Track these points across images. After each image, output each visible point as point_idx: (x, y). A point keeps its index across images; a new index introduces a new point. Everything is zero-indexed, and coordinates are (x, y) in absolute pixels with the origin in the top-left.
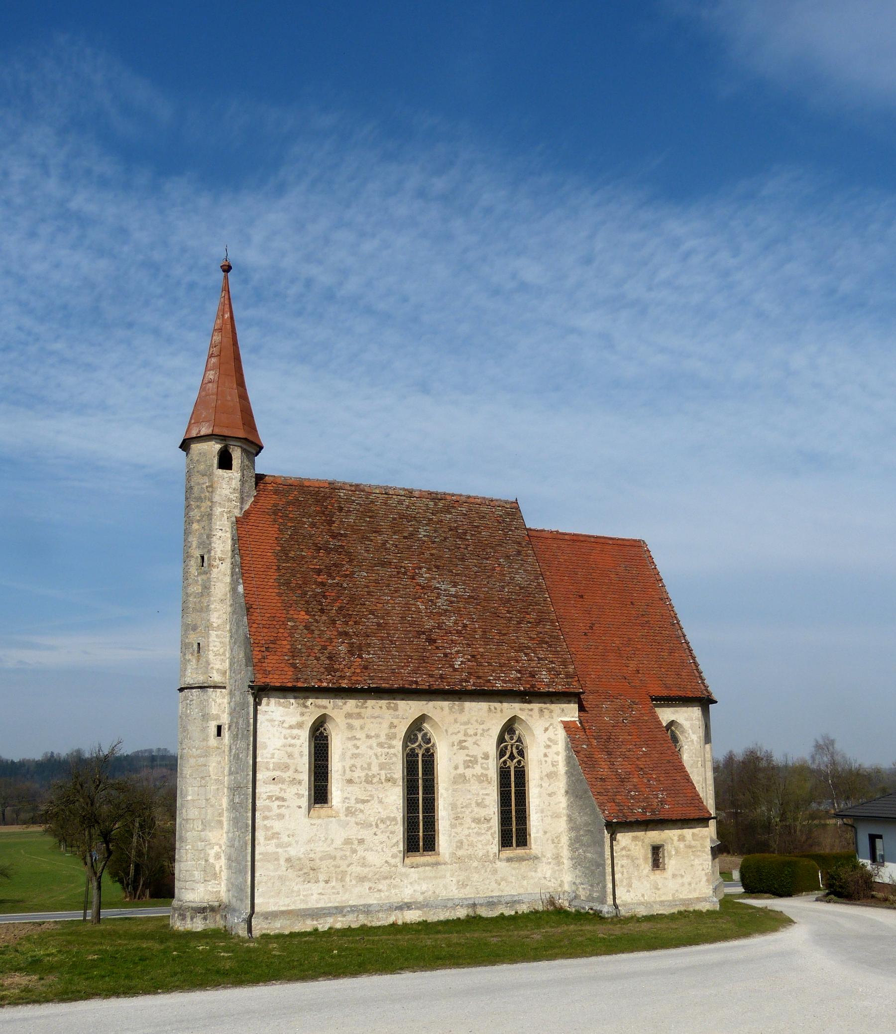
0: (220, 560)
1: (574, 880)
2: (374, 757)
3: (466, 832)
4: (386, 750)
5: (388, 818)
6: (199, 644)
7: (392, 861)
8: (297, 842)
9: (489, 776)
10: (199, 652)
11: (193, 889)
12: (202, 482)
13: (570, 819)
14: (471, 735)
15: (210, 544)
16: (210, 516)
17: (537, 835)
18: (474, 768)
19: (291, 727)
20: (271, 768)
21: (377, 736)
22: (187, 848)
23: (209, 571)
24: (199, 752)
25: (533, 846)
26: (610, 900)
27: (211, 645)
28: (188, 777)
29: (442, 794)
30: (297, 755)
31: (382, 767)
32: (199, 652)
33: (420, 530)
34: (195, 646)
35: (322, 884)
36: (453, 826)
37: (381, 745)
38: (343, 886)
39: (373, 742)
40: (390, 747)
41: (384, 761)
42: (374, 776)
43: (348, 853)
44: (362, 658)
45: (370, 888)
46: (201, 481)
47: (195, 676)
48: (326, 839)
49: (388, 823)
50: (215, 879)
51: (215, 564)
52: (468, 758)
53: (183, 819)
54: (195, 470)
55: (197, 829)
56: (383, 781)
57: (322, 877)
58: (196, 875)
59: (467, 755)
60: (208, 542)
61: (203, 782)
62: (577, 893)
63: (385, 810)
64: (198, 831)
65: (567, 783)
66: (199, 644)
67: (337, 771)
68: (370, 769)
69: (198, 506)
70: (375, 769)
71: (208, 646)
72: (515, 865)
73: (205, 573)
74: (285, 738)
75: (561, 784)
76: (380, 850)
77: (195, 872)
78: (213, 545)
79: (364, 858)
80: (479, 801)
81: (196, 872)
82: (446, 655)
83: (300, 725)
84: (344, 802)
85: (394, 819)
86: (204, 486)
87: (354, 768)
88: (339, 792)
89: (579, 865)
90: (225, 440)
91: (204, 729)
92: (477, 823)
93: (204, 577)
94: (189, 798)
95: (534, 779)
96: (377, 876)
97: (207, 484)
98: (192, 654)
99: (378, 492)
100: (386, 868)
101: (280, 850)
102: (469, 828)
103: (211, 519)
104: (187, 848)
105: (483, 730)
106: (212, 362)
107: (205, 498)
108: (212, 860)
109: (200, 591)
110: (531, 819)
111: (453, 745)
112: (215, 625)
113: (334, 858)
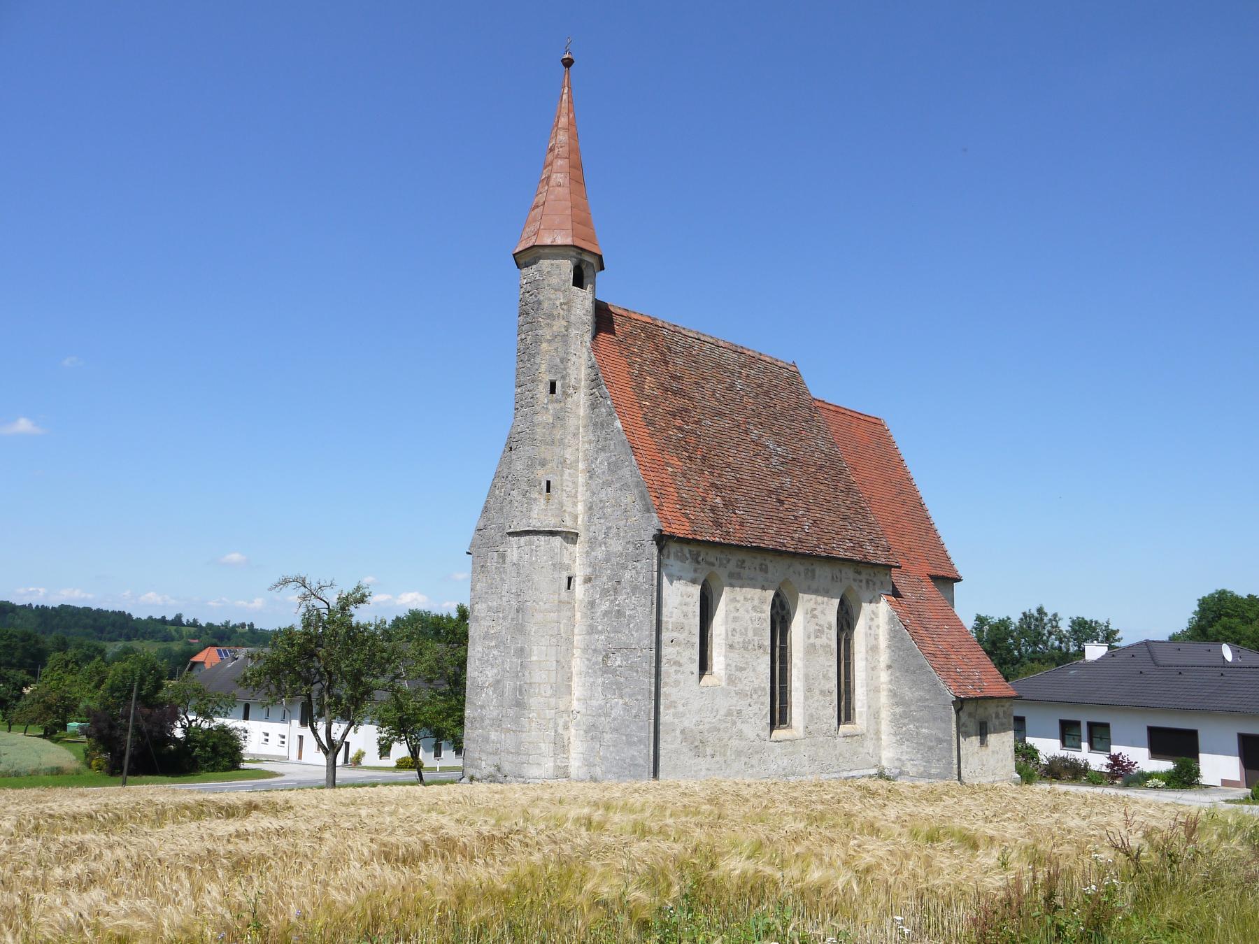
2: (749, 622)
3: (815, 705)
4: (760, 615)
5: (760, 687)
6: (548, 483)
8: (690, 711)
9: (832, 647)
10: (548, 490)
11: (538, 764)
13: (893, 694)
14: (819, 604)
15: (565, 369)
17: (862, 710)
18: (821, 638)
21: (752, 599)
22: (530, 716)
24: (547, 606)
28: (533, 634)
29: (795, 664)
30: (690, 615)
31: (756, 632)
32: (548, 490)
34: (544, 485)
35: (709, 758)
36: (806, 698)
37: (755, 609)
39: (749, 605)
41: (757, 626)
42: (749, 642)
43: (729, 725)
45: (745, 763)
46: (553, 297)
49: (760, 693)
52: (817, 627)
54: (546, 282)
55: (544, 694)
57: (709, 751)
58: (543, 748)
59: (817, 624)
60: (562, 367)
62: (903, 768)
63: (757, 678)
64: (546, 697)
65: (890, 657)
66: (548, 483)
67: (720, 635)
68: (746, 634)
69: (548, 324)
70: (750, 633)
73: (558, 401)
75: (884, 657)
81: (542, 745)
85: (764, 689)
86: (558, 303)
87: (734, 633)
88: (722, 659)
89: (908, 740)
90: (580, 254)
92: (824, 696)
93: (558, 406)
94: (534, 658)
95: (860, 652)
96: (751, 750)
97: (561, 301)
100: (757, 742)
101: (676, 721)
106: (559, 164)
107: (558, 317)
108: (560, 730)
109: (551, 421)
111: (807, 613)
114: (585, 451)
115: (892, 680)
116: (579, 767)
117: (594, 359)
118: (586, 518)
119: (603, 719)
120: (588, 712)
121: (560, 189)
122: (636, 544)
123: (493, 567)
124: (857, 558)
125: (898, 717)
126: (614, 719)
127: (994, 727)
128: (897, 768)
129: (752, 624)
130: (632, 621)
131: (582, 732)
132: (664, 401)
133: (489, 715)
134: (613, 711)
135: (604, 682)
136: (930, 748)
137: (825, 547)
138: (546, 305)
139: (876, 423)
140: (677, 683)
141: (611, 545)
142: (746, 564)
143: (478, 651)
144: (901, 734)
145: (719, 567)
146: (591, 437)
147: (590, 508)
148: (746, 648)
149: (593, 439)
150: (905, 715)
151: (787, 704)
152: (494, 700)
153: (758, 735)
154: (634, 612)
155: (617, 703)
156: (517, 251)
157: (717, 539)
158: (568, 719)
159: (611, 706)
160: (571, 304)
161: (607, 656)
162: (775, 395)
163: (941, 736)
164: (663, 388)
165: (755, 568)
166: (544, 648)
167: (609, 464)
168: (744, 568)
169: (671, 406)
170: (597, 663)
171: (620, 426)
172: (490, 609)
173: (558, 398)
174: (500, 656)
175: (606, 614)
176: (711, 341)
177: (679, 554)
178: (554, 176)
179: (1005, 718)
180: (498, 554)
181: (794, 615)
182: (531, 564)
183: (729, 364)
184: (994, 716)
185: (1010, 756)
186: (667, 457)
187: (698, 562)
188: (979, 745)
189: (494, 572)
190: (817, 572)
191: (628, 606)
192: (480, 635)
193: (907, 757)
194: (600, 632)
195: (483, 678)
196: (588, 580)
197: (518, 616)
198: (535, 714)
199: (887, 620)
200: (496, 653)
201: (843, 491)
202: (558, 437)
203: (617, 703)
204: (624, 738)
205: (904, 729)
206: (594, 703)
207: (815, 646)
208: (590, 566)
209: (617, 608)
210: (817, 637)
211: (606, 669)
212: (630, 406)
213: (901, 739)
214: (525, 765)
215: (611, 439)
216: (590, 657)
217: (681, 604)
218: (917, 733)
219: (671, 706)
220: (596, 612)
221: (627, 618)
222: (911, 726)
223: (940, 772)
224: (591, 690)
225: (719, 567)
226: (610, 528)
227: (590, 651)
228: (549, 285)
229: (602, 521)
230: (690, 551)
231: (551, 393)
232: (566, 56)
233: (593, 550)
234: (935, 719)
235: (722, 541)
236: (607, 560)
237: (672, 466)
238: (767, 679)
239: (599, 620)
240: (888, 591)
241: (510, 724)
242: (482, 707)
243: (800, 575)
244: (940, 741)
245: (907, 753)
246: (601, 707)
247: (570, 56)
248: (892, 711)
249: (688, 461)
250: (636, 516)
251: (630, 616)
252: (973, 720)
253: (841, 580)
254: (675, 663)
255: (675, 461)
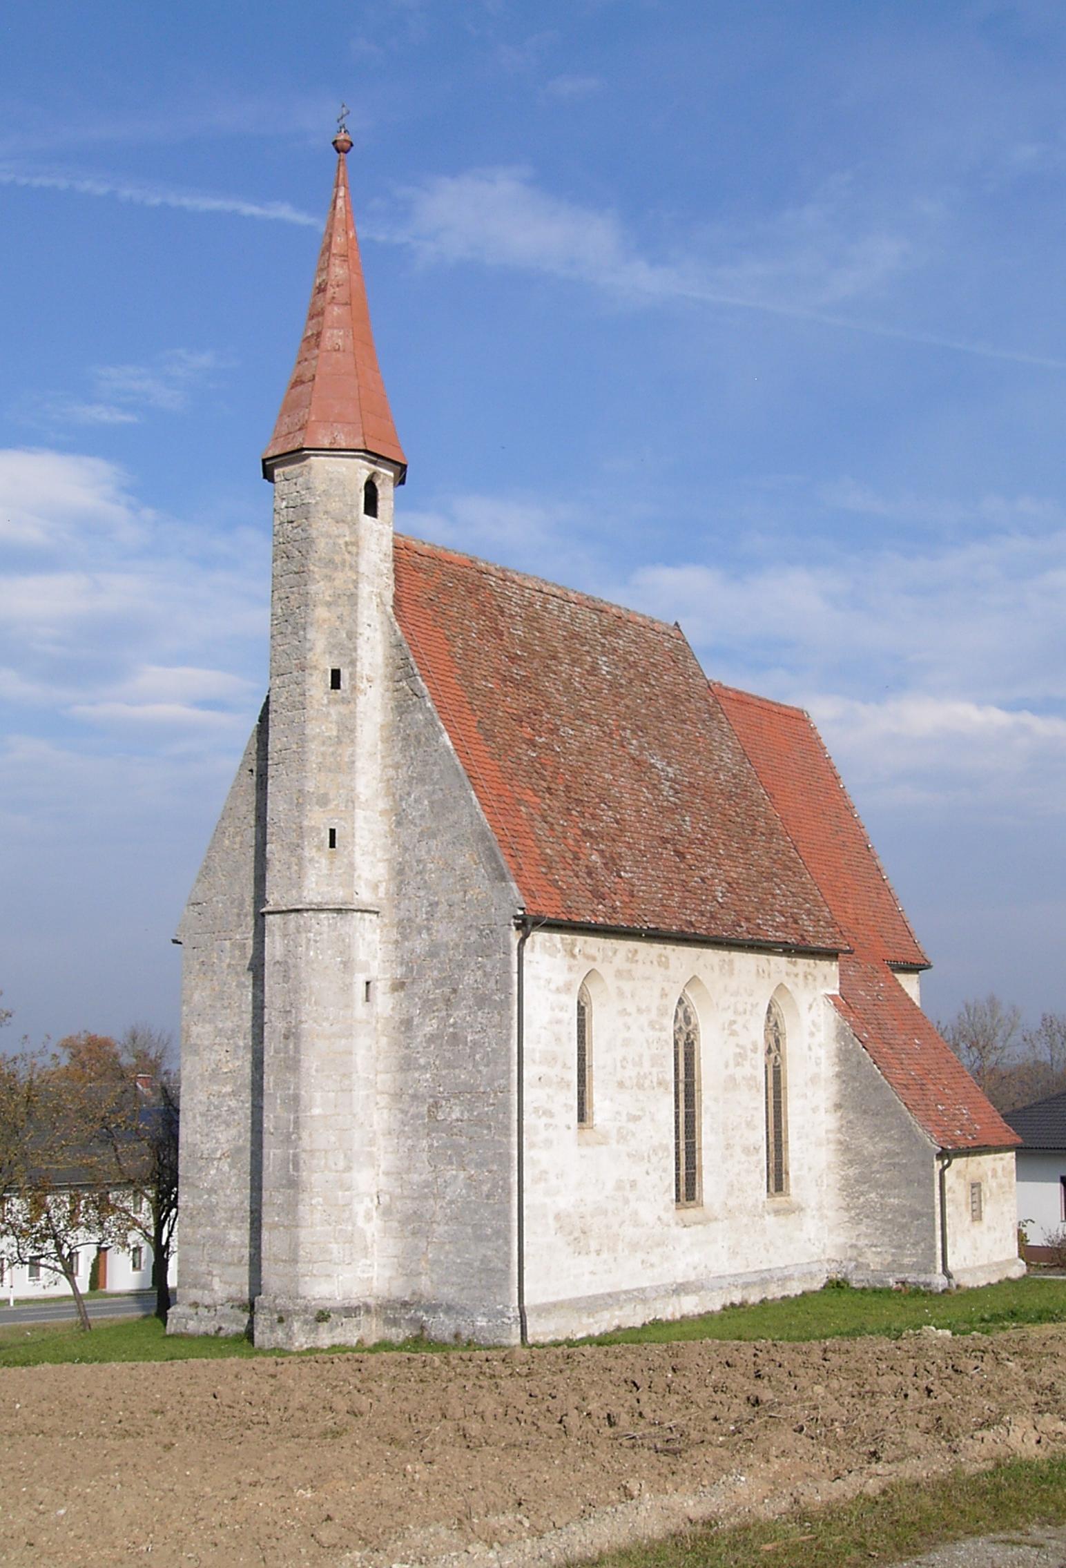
0: (369, 681)
1: (854, 1241)
4: (658, 1034)
6: (332, 832)
7: (665, 1216)
10: (332, 845)
11: (329, 1276)
12: (336, 532)
15: (355, 649)
16: (353, 598)
18: (743, 1065)
19: (558, 990)
20: (538, 1059)
21: (648, 1010)
22: (314, 1202)
23: (354, 700)
25: (792, 1190)
26: (940, 1269)
27: (358, 834)
28: (314, 1073)
31: (655, 1061)
32: (332, 845)
33: (600, 662)
35: (593, 1255)
37: (652, 1024)
38: (615, 1259)
40: (662, 1029)
44: (621, 877)
45: (643, 1262)
47: (325, 889)
48: (597, 1181)
50: (366, 1257)
51: (362, 687)
52: (738, 1050)
53: (304, 1151)
54: (321, 508)
55: (333, 1167)
56: (655, 1084)
57: (594, 1245)
58: (335, 1251)
59: (737, 1045)
60: (351, 646)
61: (347, 1082)
62: (860, 1260)
64: (337, 1171)
65: (839, 1091)
66: (332, 832)
68: (641, 1064)
71: (353, 836)
72: (782, 1219)
73: (346, 701)
74: (553, 1009)
76: (653, 1199)
77: (331, 1245)
78: (359, 652)
79: (636, 1213)
80: (749, 1119)
81: (334, 1247)
82: (703, 879)
83: (567, 988)
84: (615, 1119)
85: (756, 1149)
86: (341, 541)
87: (625, 1063)
89: (868, 1217)
90: (374, 463)
91: (347, 988)
92: (747, 1155)
93: (342, 709)
94: (316, 1111)
97: (347, 539)
98: (319, 848)
99: (530, 586)
102: (739, 1162)
103: (356, 604)
104: (314, 1202)
105: (752, 1005)
109: (335, 733)
110: (790, 1148)
111: (724, 1029)
112: (363, 798)
113: (605, 1213)
114: (388, 780)
115: (842, 1126)
116: (390, 1278)
117: (399, 633)
118: (393, 889)
119: (432, 1202)
120: (406, 1193)
121: (339, 355)
122: (481, 931)
123: (224, 965)
124: (792, 940)
125: (852, 1182)
126: (451, 1202)
127: (990, 1191)
128: (850, 1260)
129: (649, 1048)
130: (478, 1050)
131: (395, 1224)
132: (502, 698)
133: (225, 1202)
134: (448, 1190)
135: (431, 1146)
136: (903, 1227)
137: (748, 925)
138: (322, 545)
139: (798, 718)
140: (548, 1143)
141: (438, 931)
142: (640, 957)
143: (200, 1102)
144: (857, 1208)
145: (603, 962)
146: (398, 757)
147: (401, 872)
148: (640, 1087)
149: (402, 762)
150: (861, 1179)
151: (695, 1168)
152: (233, 1180)
153: (659, 1219)
154: (482, 1035)
155: (456, 1177)
156: (270, 454)
157: (601, 919)
158: (370, 1205)
159: (445, 1181)
160: (360, 543)
161: (436, 1105)
162: (656, 679)
163: (919, 1208)
164: (499, 677)
165: (652, 962)
166: (332, 1095)
167: (432, 803)
168: (637, 961)
169: (515, 706)
170: (417, 1116)
171: (449, 743)
172: (219, 1032)
173: (345, 695)
174: (241, 1109)
175: (431, 1039)
176: (558, 593)
177: (548, 944)
178: (327, 334)
179: (1004, 1176)
180: (232, 944)
181: (844, 1056)
182: (308, 963)
183: (587, 632)
184: (990, 1174)
185: (1011, 1234)
186: (517, 789)
187: (573, 956)
188: (970, 1218)
189: (226, 972)
190: (737, 965)
191: (472, 1027)
192: (201, 1075)
193: (866, 1242)
194: (424, 1068)
195: (212, 1144)
196: (399, 986)
197: (286, 1046)
198: (320, 1199)
199: (834, 1034)
200: (233, 1103)
201: (763, 834)
202: (346, 760)
203: (456, 1177)
204: (469, 1230)
205: (862, 1199)
206: (415, 1177)
207: (735, 1079)
208: (402, 964)
209: (451, 1030)
210: (738, 1064)
211: (433, 1123)
212: (457, 708)
213: (858, 1215)
214: (307, 1278)
215: (435, 764)
216: (405, 1107)
217: (551, 1023)
218: (881, 1204)
219: (540, 1179)
220: (416, 1037)
221: (469, 1044)
222: (872, 1195)
223: (917, 1262)
224: (410, 1158)
225: (603, 962)
226: (437, 903)
227: (407, 1098)
228: (326, 512)
229: (422, 893)
230: (562, 939)
231: (333, 687)
232: (342, 137)
233: (405, 937)
234: (910, 1183)
235: (608, 922)
236: (433, 954)
237: (526, 804)
238: (670, 1131)
239: (421, 1049)
240: (834, 989)
241: (278, 1215)
242: (211, 1191)
243: (712, 969)
244: (916, 1215)
245: (866, 1235)
246: (427, 1185)
247: (348, 138)
248: (843, 1173)
249: (548, 796)
250: (481, 886)
251: (475, 1043)
252: (962, 1181)
253: (769, 975)
254: (544, 1113)
255: (529, 796)
